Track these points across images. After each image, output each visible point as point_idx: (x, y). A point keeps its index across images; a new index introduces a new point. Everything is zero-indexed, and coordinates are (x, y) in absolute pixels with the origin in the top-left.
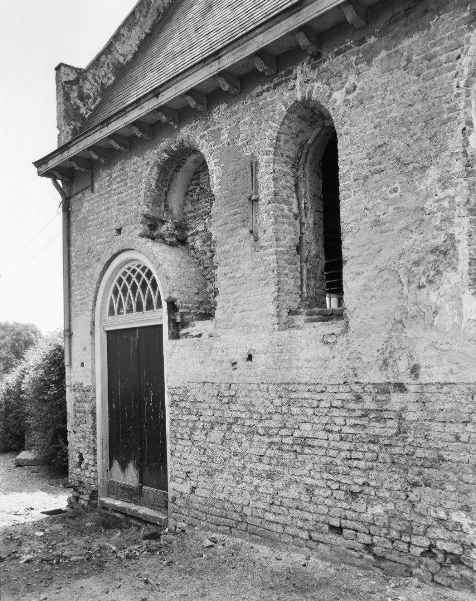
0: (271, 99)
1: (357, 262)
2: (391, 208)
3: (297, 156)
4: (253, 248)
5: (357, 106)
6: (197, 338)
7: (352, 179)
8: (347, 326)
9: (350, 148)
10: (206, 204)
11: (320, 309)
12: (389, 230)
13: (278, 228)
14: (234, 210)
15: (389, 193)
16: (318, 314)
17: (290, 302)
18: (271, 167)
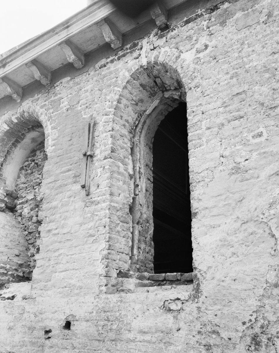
0: (114, 69)
1: (212, 214)
2: (255, 154)
3: (135, 123)
4: (84, 204)
5: (210, 62)
6: (9, 301)
7: (204, 128)
8: (197, 290)
9: (201, 99)
10: (38, 176)
11: (150, 274)
12: (252, 177)
13: (113, 183)
14: (66, 168)
15: (251, 138)
16: (149, 279)
17: (121, 263)
18: (110, 125)
